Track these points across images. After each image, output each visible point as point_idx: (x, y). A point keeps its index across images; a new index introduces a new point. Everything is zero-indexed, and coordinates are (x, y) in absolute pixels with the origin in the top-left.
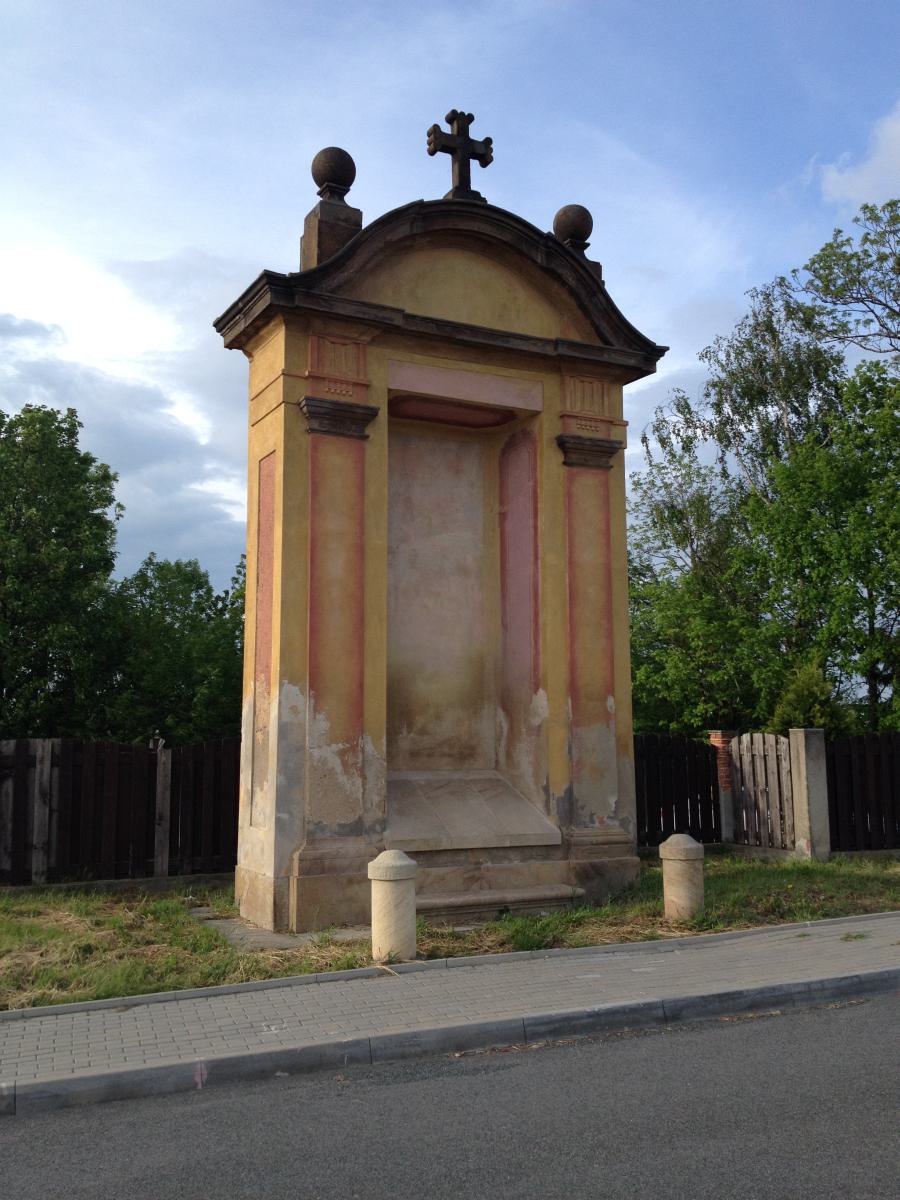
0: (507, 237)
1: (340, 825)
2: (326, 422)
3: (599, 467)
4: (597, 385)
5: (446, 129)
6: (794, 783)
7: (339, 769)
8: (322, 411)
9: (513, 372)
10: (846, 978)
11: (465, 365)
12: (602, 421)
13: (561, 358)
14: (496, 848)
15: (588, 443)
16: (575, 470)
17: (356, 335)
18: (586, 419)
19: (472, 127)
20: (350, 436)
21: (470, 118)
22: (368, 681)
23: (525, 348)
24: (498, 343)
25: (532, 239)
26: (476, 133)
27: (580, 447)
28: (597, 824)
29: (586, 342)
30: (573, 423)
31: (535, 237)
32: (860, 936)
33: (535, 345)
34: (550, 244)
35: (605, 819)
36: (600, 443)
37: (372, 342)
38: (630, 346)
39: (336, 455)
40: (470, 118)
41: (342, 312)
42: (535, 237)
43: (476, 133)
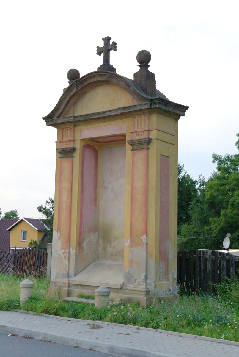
1: (63, 274)
3: (71, 157)
4: (146, 117)
5: (111, 43)
6: (52, 263)
7: (63, 257)
8: (61, 151)
9: (117, 121)
10: (141, 351)
13: (121, 114)
14: (93, 286)
15: (136, 141)
16: (135, 152)
17: (69, 126)
18: (138, 132)
20: (69, 157)
22: (72, 231)
23: (110, 114)
24: (102, 116)
25: (110, 75)
27: (134, 143)
28: (137, 284)
29: (141, 103)
30: (134, 134)
31: (111, 75)
32: (137, 332)
33: (114, 112)
35: (140, 282)
37: (75, 126)
38: (144, 102)
39: (66, 163)
42: (111, 75)
43: (101, 44)
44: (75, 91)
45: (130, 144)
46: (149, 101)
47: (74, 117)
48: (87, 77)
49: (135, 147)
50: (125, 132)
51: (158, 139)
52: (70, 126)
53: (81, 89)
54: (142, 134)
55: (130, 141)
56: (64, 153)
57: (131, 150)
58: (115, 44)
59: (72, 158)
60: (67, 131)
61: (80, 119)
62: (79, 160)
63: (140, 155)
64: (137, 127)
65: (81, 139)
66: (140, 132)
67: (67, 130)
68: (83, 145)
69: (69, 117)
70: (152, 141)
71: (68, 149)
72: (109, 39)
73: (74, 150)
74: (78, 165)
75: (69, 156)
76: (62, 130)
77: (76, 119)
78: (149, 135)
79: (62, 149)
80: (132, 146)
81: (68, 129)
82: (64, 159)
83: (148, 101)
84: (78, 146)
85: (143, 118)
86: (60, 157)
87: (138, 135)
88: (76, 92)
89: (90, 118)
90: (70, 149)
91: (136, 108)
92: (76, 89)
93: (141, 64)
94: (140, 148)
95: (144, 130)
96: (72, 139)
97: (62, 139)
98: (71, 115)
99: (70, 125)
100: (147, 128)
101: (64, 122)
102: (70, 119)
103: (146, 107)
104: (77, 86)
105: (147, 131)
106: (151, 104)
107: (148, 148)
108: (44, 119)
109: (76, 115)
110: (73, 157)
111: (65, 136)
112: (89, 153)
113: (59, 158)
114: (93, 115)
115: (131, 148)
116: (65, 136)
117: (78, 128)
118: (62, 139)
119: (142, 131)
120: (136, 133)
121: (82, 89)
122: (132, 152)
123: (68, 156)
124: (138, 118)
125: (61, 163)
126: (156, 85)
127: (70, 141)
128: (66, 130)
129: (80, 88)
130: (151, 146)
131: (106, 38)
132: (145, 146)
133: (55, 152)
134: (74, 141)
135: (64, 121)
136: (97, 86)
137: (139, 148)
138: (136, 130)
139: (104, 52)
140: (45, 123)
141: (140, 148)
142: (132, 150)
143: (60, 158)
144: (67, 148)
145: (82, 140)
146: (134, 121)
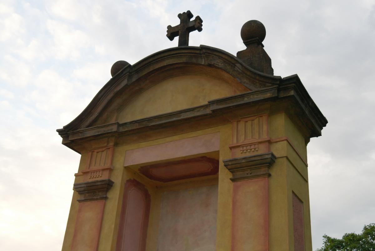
0: (184, 60)
2: (87, 195)
8: (83, 189)
9: (200, 132)
11: (168, 139)
12: (260, 143)
15: (243, 161)
16: (239, 183)
17: (106, 144)
18: (246, 145)
19: (173, 25)
20: (97, 199)
21: (200, 30)
25: (196, 53)
26: (176, 22)
27: (239, 166)
29: (239, 93)
33: (198, 111)
34: (204, 51)
36: (254, 159)
37: (116, 144)
38: (265, 86)
39: (91, 212)
40: (200, 30)
41: (88, 135)
43: (176, 22)
44: (126, 83)
45: (229, 167)
46: (276, 84)
47: (119, 125)
48: (151, 60)
49: (239, 174)
50: (217, 150)
51: (290, 159)
52: (108, 144)
53: (136, 81)
54: (255, 149)
55: (230, 161)
56: (88, 191)
57: (231, 179)
58: (199, 20)
59: (104, 201)
60: (99, 154)
61: (130, 129)
62: (116, 204)
63: (251, 189)
64: (243, 137)
65: (125, 167)
66: (250, 145)
67: (101, 152)
68: (128, 179)
69: (109, 125)
70: (277, 161)
71: (99, 184)
72: (189, 15)
73: (108, 185)
74: (115, 213)
75: (98, 197)
76: (90, 153)
77: (122, 129)
78: (269, 149)
79: (86, 184)
80: (232, 173)
81: (103, 151)
82: (88, 203)
83: (273, 84)
84: (118, 179)
85: (256, 121)
86: (79, 199)
87: (247, 150)
88: (126, 86)
89: (150, 125)
90: (103, 183)
91: (246, 99)
92: (128, 80)
93: (247, 41)
94: (252, 175)
95: (260, 140)
96: (108, 166)
97: (89, 168)
98: (113, 121)
99: (108, 142)
100: (265, 137)
101: (97, 134)
102: (110, 128)
103: (268, 95)
104: (130, 77)
105: (267, 144)
106: (279, 90)
107: (270, 175)
108: (60, 132)
109: (121, 122)
110: (106, 198)
111: (95, 163)
112: (134, 195)
113: (78, 202)
114: (157, 119)
115: (231, 176)
116: (95, 163)
117: (122, 149)
118: (89, 168)
119: (254, 144)
120: (241, 149)
121: (139, 80)
122: (232, 184)
123: (95, 198)
124: (247, 122)
125: (80, 211)
126: (274, 72)
127: (104, 170)
128: (98, 152)
129: (134, 79)
130: (274, 172)
131: (184, 13)
132: (263, 171)
133: (71, 192)
134: (111, 170)
135: (98, 132)
136: (164, 79)
137: (249, 175)
138: (242, 141)
139: (180, 33)
140: (60, 139)
141: (252, 175)
142: (233, 180)
143: (79, 201)
144: (97, 182)
145: (127, 169)
146: (237, 127)
